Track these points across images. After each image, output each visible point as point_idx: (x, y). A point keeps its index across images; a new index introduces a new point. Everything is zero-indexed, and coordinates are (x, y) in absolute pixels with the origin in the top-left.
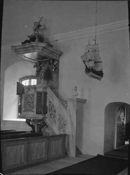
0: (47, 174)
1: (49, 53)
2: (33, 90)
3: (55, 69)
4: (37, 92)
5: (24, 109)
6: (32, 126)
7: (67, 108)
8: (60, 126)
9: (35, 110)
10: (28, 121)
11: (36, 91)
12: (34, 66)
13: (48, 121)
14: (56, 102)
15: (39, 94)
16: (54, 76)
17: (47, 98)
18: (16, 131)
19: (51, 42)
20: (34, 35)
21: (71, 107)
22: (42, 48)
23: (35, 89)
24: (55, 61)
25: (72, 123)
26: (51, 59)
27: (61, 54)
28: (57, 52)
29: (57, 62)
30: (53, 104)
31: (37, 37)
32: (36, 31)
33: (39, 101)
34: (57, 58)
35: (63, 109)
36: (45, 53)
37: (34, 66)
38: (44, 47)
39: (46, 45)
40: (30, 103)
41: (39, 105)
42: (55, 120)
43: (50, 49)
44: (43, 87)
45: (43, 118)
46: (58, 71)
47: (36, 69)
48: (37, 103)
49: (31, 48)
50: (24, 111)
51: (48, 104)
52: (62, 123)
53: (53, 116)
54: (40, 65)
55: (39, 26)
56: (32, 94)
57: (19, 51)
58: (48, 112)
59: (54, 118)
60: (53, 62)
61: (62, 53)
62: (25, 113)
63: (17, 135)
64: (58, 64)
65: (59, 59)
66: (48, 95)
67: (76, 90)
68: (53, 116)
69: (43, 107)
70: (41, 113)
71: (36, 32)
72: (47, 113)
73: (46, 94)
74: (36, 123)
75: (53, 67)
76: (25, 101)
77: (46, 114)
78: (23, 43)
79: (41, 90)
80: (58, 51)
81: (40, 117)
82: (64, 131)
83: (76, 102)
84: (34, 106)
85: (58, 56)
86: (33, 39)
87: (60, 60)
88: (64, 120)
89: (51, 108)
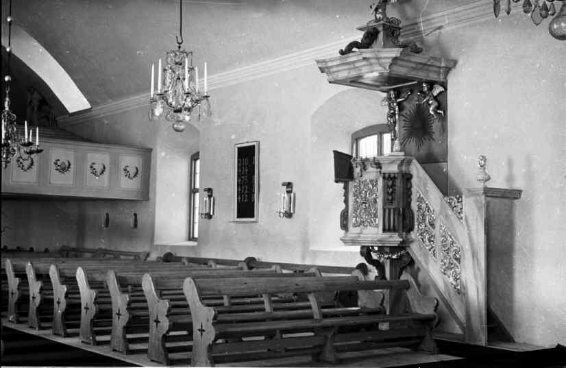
0: (401, 367)
1: (414, 69)
2: (375, 170)
3: (438, 108)
4: (384, 174)
5: (354, 219)
6: (380, 266)
7: (462, 215)
8: (445, 264)
9: (379, 221)
10: (365, 250)
11: (380, 172)
13: (415, 250)
14: (433, 197)
15: (388, 178)
16: (436, 125)
17: (414, 190)
19: (427, 32)
20: (373, 24)
21: (472, 211)
22: (390, 61)
24: (435, 86)
25: (474, 255)
26: (426, 83)
27: (451, 65)
28: (438, 64)
29: (441, 89)
31: (381, 29)
32: (380, 13)
33: (390, 198)
34: (441, 78)
35: (453, 217)
38: (395, 59)
39: (401, 53)
40: (367, 205)
41: (389, 210)
42: (433, 247)
43: (417, 58)
44: (399, 162)
45: (403, 242)
46: (444, 112)
48: (384, 204)
49: (364, 63)
50: (355, 226)
51: (414, 205)
52: (451, 255)
53: (427, 236)
54: (397, 97)
56: (371, 181)
58: (416, 227)
59: (430, 241)
60: (431, 89)
61: (455, 62)
62: (357, 230)
63: (345, 311)
64: (443, 94)
65: (445, 78)
66: (414, 181)
67: (485, 165)
69: (401, 215)
70: (394, 230)
71: (378, 16)
72: (411, 229)
73: (407, 178)
74: (386, 256)
75: (430, 102)
76: (355, 199)
77: (412, 232)
78: (342, 53)
79: (394, 169)
80: (439, 60)
81: (395, 239)
83: (483, 197)
85: (442, 71)
87: (449, 82)
89: (423, 215)
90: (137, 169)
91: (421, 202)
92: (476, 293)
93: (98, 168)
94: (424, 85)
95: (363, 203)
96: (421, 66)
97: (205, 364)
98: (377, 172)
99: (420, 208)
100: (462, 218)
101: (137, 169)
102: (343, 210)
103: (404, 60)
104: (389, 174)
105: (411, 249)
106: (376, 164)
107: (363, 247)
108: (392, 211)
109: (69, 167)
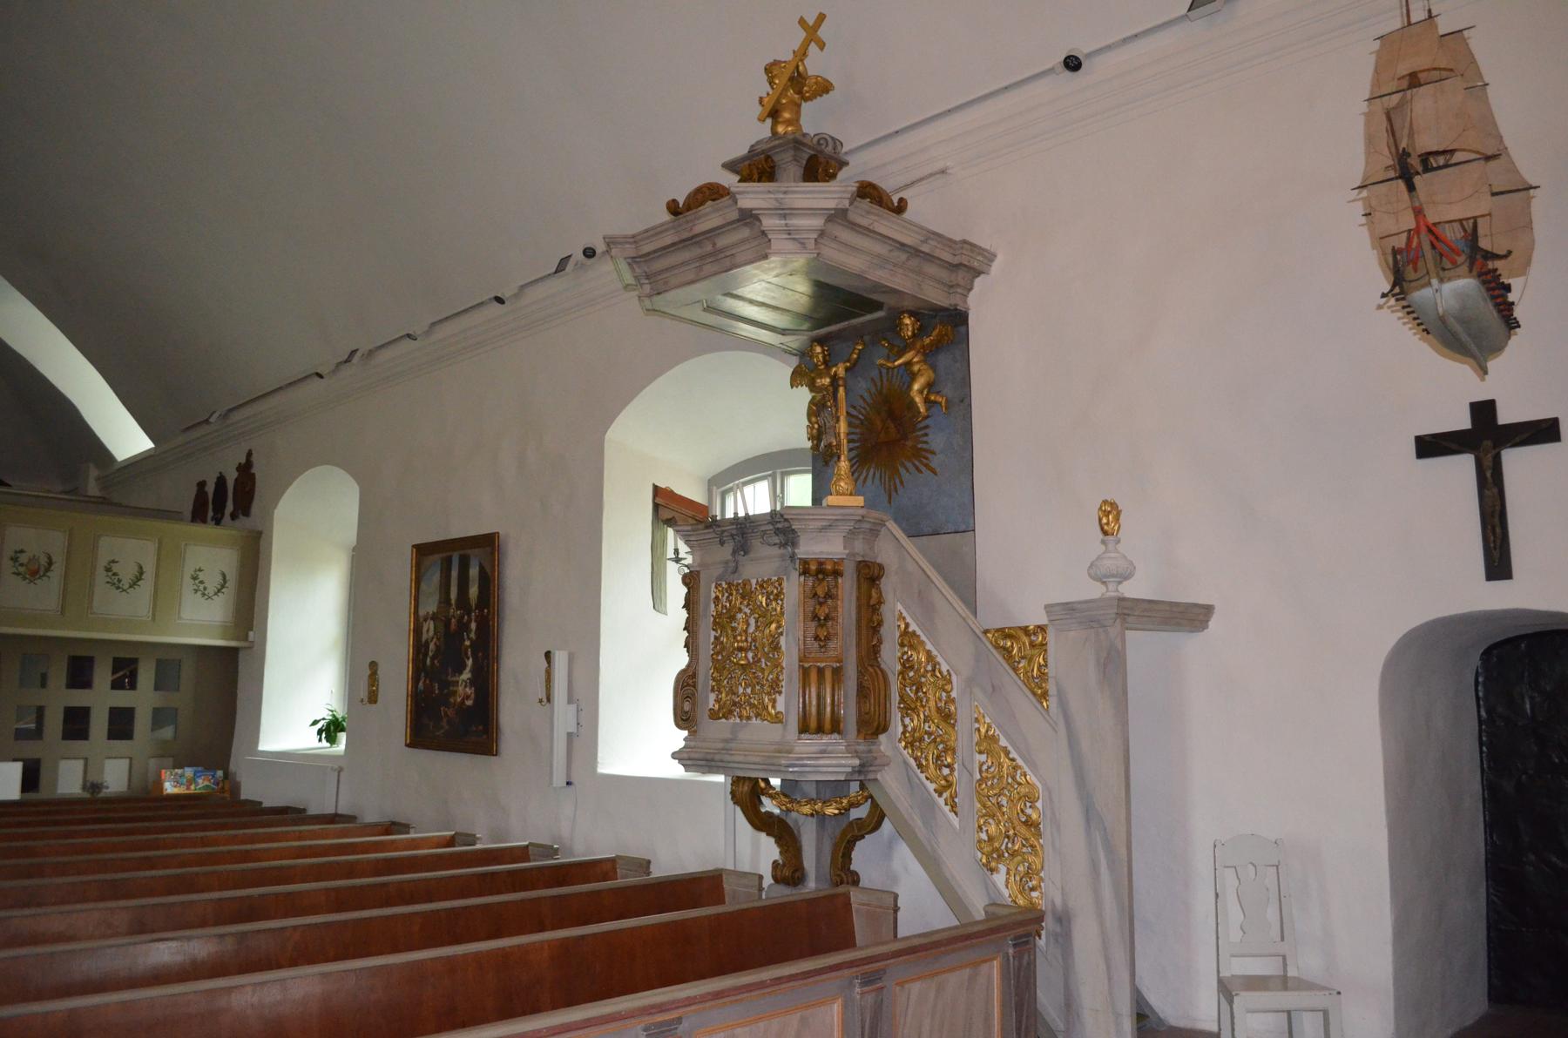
2: (776, 551)
4: (805, 562)
5: (712, 697)
11: (793, 557)
12: (797, 378)
15: (820, 573)
18: (659, 871)
23: (783, 545)
26: (912, 314)
30: (928, 653)
36: (858, 260)
37: (797, 378)
40: (750, 655)
43: (886, 224)
47: (804, 395)
49: (745, 232)
50: (714, 715)
51: (890, 656)
55: (798, 80)
57: (661, 272)
68: (933, 749)
69: (866, 685)
72: (883, 728)
73: (870, 575)
77: (882, 738)
79: (829, 547)
81: (829, 759)
82: (1029, 874)
84: (783, 677)
86: (758, 167)
88: (1023, 790)
90: (224, 576)
91: (911, 647)
92: (1262, 1016)
93: (126, 572)
94: (907, 321)
95: (740, 649)
96: (904, 257)
97: (962, 329)
98: (782, 557)
99: (907, 665)
100: (1045, 695)
101: (224, 576)
102: (683, 672)
103: (854, 226)
104: (821, 563)
105: (881, 788)
106: (777, 532)
107: (737, 781)
108: (828, 674)
109: (47, 570)
